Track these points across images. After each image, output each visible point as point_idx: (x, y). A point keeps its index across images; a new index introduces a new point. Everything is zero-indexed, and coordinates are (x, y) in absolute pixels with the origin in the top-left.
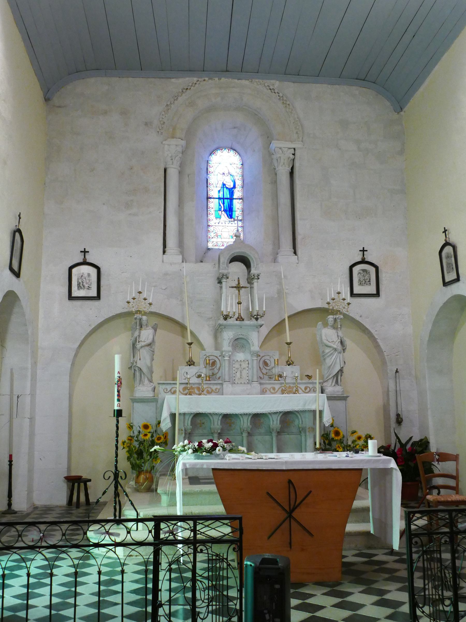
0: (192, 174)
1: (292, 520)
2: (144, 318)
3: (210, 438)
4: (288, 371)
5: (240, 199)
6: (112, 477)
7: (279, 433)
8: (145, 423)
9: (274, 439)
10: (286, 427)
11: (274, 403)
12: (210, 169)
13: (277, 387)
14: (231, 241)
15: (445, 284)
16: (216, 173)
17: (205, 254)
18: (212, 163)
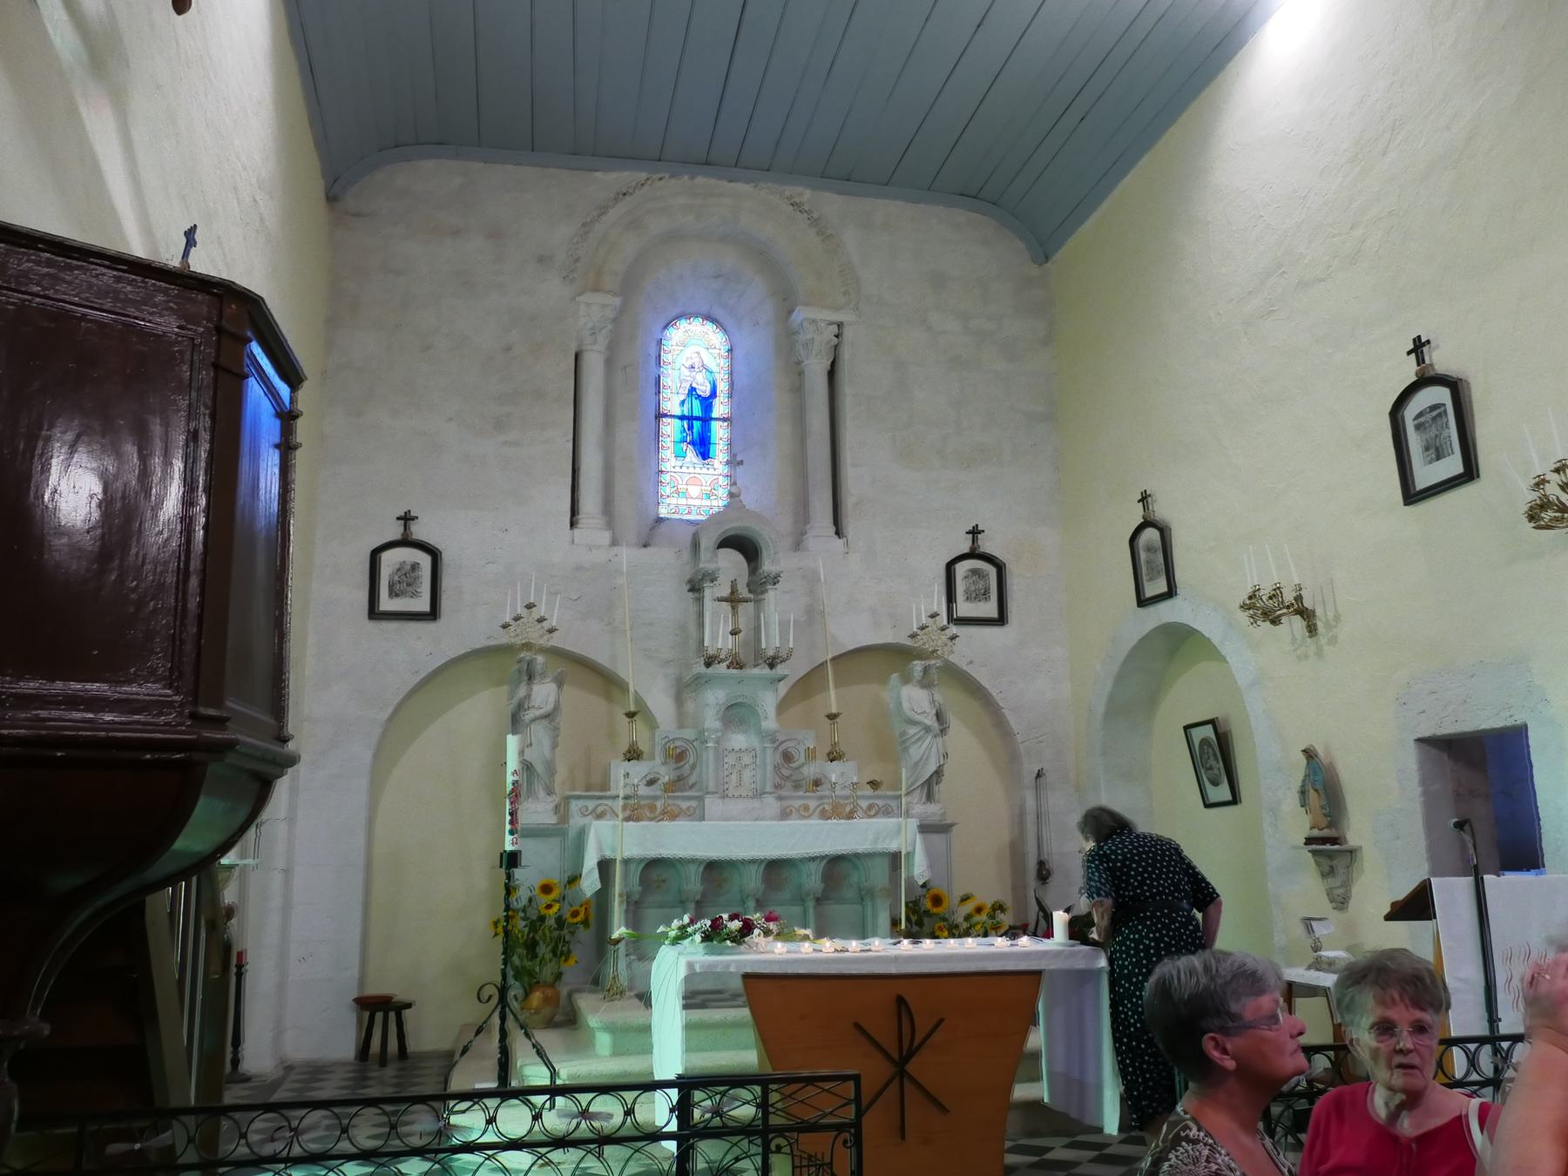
0: (634, 366)
1: (906, 1082)
2: (540, 659)
3: (735, 910)
4: (834, 772)
5: (724, 420)
6: (495, 1000)
7: (819, 901)
8: (545, 881)
9: (811, 911)
10: (833, 890)
11: (807, 837)
12: (664, 357)
13: (812, 804)
14: (719, 502)
15: (1142, 602)
16: (677, 366)
17: (654, 530)
18: (668, 345)
